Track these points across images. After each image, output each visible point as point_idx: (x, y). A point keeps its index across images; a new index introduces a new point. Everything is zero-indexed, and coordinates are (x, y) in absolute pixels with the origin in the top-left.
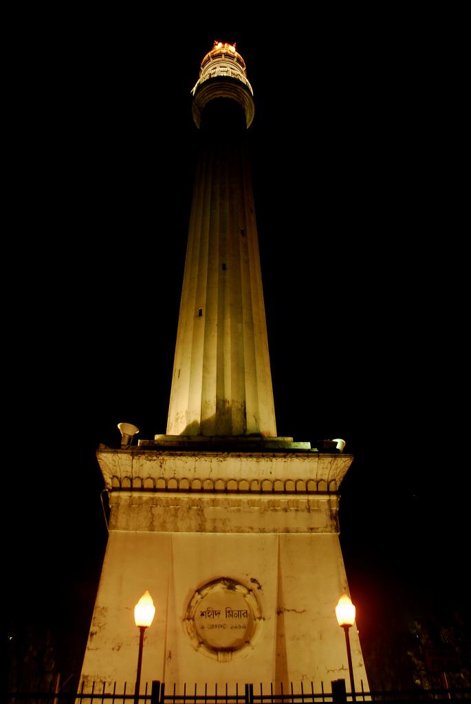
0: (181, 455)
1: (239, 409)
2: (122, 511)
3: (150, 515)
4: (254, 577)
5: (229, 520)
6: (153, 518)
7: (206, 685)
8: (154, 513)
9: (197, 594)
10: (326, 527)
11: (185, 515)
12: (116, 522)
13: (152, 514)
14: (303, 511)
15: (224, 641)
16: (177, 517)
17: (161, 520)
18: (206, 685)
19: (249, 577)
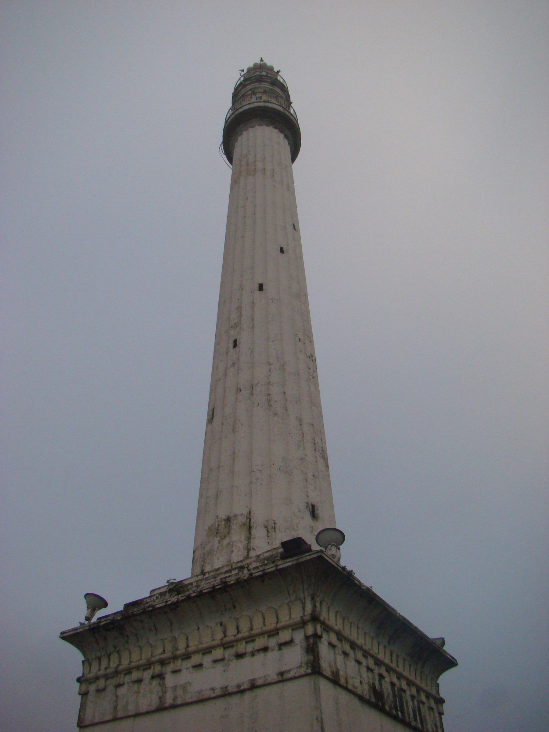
1: (244, 524)
6: (116, 701)
16: (140, 692)
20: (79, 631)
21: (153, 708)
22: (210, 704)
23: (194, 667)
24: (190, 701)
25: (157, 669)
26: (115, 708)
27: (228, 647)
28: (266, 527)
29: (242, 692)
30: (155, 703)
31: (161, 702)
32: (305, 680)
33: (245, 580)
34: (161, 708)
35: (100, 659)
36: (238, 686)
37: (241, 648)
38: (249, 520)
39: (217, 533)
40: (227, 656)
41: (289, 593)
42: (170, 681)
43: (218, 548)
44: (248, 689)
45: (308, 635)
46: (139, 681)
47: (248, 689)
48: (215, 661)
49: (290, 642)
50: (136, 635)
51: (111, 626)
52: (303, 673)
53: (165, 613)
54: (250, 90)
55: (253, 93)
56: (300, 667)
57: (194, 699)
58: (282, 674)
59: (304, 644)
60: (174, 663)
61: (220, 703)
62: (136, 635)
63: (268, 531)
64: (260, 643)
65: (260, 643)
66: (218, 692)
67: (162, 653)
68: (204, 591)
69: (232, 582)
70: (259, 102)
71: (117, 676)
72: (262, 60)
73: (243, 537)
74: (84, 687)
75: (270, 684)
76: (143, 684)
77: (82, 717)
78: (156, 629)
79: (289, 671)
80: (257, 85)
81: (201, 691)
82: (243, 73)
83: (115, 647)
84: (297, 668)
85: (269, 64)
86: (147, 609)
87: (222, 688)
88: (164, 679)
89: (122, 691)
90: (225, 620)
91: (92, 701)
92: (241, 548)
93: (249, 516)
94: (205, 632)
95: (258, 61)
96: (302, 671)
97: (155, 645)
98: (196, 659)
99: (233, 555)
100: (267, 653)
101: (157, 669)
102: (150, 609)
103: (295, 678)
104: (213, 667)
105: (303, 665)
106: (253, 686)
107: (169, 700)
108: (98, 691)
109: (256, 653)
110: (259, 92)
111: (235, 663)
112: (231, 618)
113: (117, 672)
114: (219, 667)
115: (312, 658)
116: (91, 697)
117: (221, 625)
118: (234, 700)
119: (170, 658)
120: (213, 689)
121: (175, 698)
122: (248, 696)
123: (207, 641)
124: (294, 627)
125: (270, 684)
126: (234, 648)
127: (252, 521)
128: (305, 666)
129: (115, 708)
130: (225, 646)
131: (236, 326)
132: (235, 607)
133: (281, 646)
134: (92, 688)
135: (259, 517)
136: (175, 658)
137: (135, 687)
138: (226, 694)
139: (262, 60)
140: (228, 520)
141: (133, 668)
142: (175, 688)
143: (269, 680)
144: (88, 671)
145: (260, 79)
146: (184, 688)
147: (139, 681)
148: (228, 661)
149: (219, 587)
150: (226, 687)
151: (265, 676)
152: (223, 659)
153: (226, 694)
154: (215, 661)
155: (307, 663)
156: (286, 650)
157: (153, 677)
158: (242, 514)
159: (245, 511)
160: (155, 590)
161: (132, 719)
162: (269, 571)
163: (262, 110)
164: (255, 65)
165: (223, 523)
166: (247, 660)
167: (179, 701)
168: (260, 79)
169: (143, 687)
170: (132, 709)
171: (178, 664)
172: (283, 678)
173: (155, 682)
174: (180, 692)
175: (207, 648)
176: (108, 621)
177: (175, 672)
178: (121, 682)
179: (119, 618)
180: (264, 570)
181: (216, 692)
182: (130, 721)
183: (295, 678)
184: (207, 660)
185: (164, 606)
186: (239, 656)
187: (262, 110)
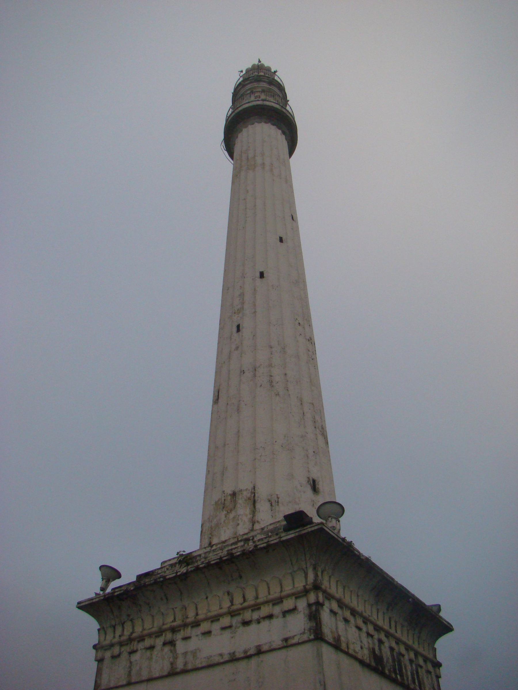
5: (200, 651)
6: (130, 667)
10: (304, 633)
13: (131, 662)
15: (328, 506)
20: (94, 601)
21: (165, 673)
24: (200, 666)
25: (169, 636)
28: (269, 501)
29: (249, 657)
30: (167, 668)
34: (173, 673)
35: (114, 627)
37: (247, 615)
38: (253, 495)
39: (223, 508)
42: (181, 647)
43: (224, 521)
49: (294, 610)
52: (307, 639)
53: (176, 583)
54: (249, 89)
56: (304, 633)
57: (204, 664)
58: (286, 640)
59: (307, 612)
61: (229, 668)
63: (271, 505)
64: (265, 610)
65: (265, 610)
66: (226, 658)
69: (239, 553)
72: (260, 61)
76: (155, 650)
78: (167, 599)
79: (293, 637)
80: (255, 85)
81: (211, 656)
83: (129, 616)
84: (301, 634)
87: (230, 654)
88: (174, 645)
89: (135, 657)
93: (253, 491)
94: (214, 601)
95: (256, 63)
96: (305, 637)
97: (167, 615)
101: (169, 636)
103: (298, 644)
105: (306, 631)
106: (259, 652)
107: (180, 665)
113: (130, 640)
114: (227, 634)
116: (107, 662)
118: (243, 664)
119: (180, 626)
120: (221, 655)
121: (185, 664)
122: (254, 661)
123: (215, 610)
124: (297, 596)
126: (241, 616)
128: (308, 633)
130: (232, 614)
132: (241, 577)
133: (285, 613)
135: (263, 492)
136: (185, 625)
137: (148, 653)
138: (233, 659)
139: (260, 61)
140: (234, 494)
141: (146, 636)
142: (185, 654)
143: (274, 646)
146: (194, 653)
150: (234, 653)
151: (270, 642)
152: (230, 627)
153: (233, 659)
155: (310, 630)
156: (289, 618)
157: (165, 644)
159: (250, 486)
162: (272, 542)
164: (254, 66)
165: (229, 497)
166: (253, 627)
167: (190, 667)
169: (156, 653)
170: (145, 675)
171: (188, 631)
172: (287, 644)
173: (167, 649)
177: (186, 639)
178: (135, 649)
179: (132, 588)
180: (268, 541)
181: (224, 657)
183: (298, 644)
184: (216, 627)
186: (246, 623)
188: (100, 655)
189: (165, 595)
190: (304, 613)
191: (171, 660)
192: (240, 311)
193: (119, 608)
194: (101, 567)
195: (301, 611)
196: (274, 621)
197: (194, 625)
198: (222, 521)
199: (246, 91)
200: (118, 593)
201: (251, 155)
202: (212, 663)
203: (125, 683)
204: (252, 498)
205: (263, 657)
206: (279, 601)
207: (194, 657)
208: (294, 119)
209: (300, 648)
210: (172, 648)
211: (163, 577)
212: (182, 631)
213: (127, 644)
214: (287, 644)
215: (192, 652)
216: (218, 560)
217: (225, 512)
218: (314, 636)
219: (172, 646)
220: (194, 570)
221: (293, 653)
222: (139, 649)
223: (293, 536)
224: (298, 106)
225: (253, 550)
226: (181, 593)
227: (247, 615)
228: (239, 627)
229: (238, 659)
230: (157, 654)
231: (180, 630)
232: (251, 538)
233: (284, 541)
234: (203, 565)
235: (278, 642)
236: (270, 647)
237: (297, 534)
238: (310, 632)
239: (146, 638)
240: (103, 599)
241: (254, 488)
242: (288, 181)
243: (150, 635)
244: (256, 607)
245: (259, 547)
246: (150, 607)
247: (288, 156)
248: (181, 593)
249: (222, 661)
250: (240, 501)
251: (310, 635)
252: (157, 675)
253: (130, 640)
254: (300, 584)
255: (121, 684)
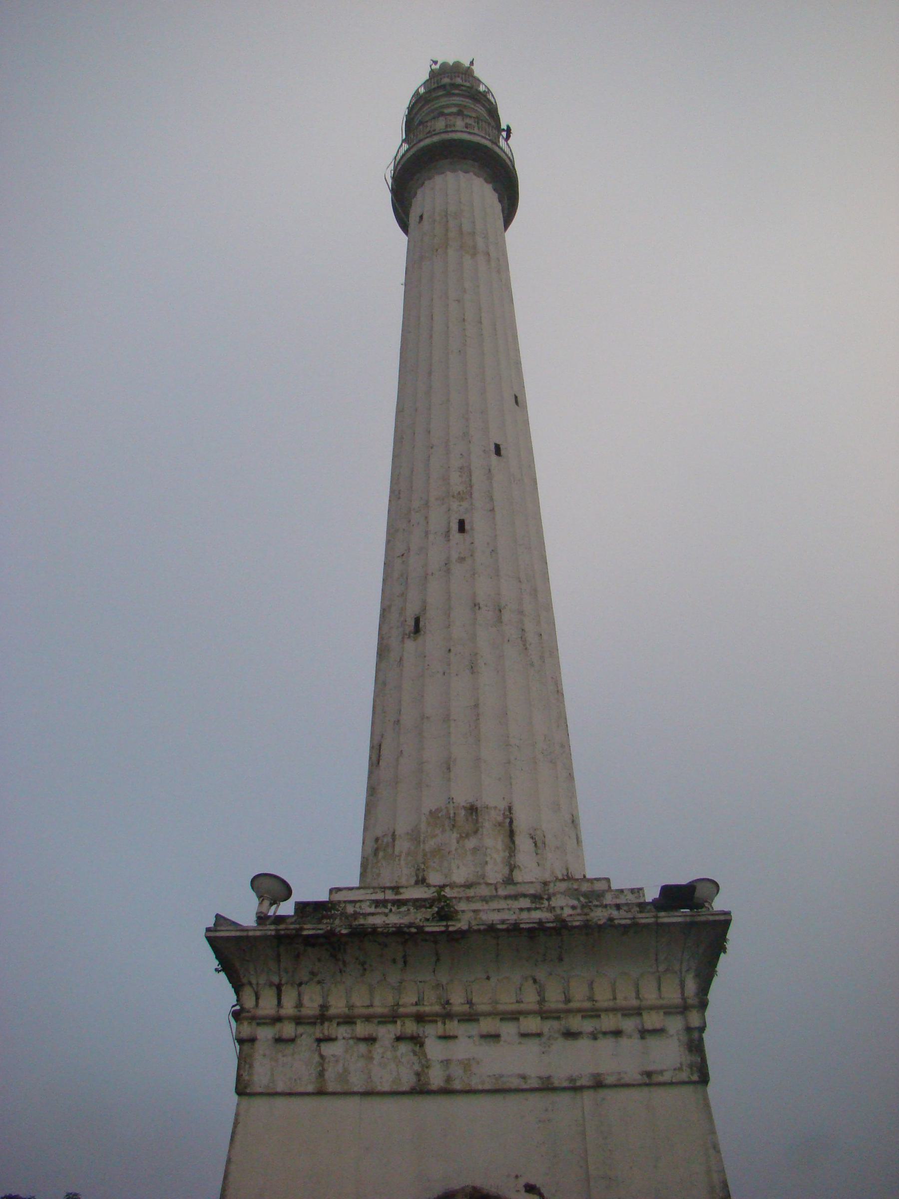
0: (370, 758)
1: (500, 824)
2: (261, 1052)
3: (317, 1058)
4: (532, 1182)
5: (478, 1063)
6: (322, 1065)
7: (516, 397)
8: (324, 1053)
9: (368, 903)
10: (680, 1069)
11: (389, 1054)
12: (250, 1074)
13: (322, 1057)
14: (630, 1037)
15: (709, 885)
16: (372, 1058)
17: (340, 1068)
18: (516, 397)
19: (522, 1182)
20: (251, 934)
21: (405, 1088)
22: (512, 1099)
23: (483, 1036)
24: (480, 1087)
25: (411, 1027)
26: (321, 1074)
27: (547, 1018)
28: (532, 838)
29: (575, 1089)
30: (407, 1080)
31: (419, 1080)
32: (691, 1088)
33: (600, 926)
34: (420, 1090)
35: (279, 988)
36: (572, 1079)
37: (576, 1023)
38: (508, 820)
39: (454, 826)
40: (546, 1030)
41: (656, 960)
42: (434, 1049)
43: (456, 850)
44: (589, 1087)
45: (692, 1026)
46: (371, 1040)
47: (589, 1087)
48: (524, 1035)
49: (659, 1032)
50: (363, 964)
51: (322, 940)
52: (687, 1079)
53: (436, 942)
54: (455, 105)
55: (460, 113)
56: (680, 1069)
57: (487, 1086)
58: (649, 1074)
59: (684, 1038)
60: (444, 1023)
61: (536, 1101)
62: (363, 964)
63: (536, 845)
64: (608, 1022)
65: (608, 1022)
66: (535, 1083)
67: (416, 1004)
68: (522, 926)
69: (577, 923)
70: (485, 138)
71: (322, 1023)
72: (472, 63)
73: (500, 846)
74: (247, 1030)
75: (627, 1085)
76: (377, 1045)
77: (246, 1077)
78: (405, 963)
79: (661, 1072)
80: (468, 102)
81: (501, 1076)
82: (434, 67)
83: (313, 974)
84: (675, 1069)
85: (477, 74)
86: (406, 930)
87: (540, 1078)
88: (422, 1045)
89: (328, 1049)
90: (541, 975)
91: (264, 1055)
92: (499, 860)
93: (507, 813)
94: (505, 986)
95: (467, 64)
96: (684, 1076)
97: (415, 990)
98: (487, 1025)
99: (489, 868)
100: (619, 1039)
101: (411, 1027)
102: (413, 930)
103: (671, 1084)
104: (520, 1043)
105: (684, 1068)
106: (598, 1084)
107: (436, 1078)
108: (279, 1040)
109: (600, 1036)
110: (471, 117)
111: (560, 1044)
112: (551, 974)
113: (322, 1017)
114: (533, 1046)
115: (699, 1059)
116: (262, 1048)
117: (535, 981)
118: (565, 1098)
119: (437, 1015)
120: (524, 1077)
121: (449, 1079)
122: (588, 1097)
123: (507, 1002)
124: (668, 1010)
125: (627, 1085)
126: (563, 1022)
127: (515, 823)
128: (689, 1070)
129: (321, 1074)
130: (545, 1014)
131: (460, 497)
132: (561, 959)
133: (644, 1033)
134: (265, 1034)
135: (522, 822)
136: (448, 1016)
137: (363, 1047)
138: (547, 1087)
139: (472, 63)
140: (472, 810)
141: (360, 1016)
142: (446, 1063)
143: (627, 1079)
144: (254, 1003)
145: (449, 90)
146: (466, 1065)
147: (371, 1040)
148: (549, 1039)
149: (551, 925)
150: (549, 1078)
151: (619, 1073)
152: (539, 1035)
153: (547, 1087)
154: (524, 1035)
155: (691, 1066)
156: (653, 1042)
157: (399, 1039)
158: (495, 808)
159: (502, 805)
160: (338, 890)
161: (357, 1099)
162: (643, 921)
163: (453, 145)
164: (457, 65)
165: (463, 812)
166: (583, 1044)
167: (457, 1085)
168: (449, 90)
169: (380, 1050)
170: (357, 1082)
171: (453, 1027)
172: (649, 1080)
173: (404, 1048)
174: (457, 1071)
175: (512, 1013)
176: (320, 932)
177: (445, 1037)
178: (334, 1036)
179: (344, 931)
180: (634, 918)
181: (529, 1081)
182: (352, 1103)
183: (671, 1084)
184: (508, 1030)
185: (442, 932)
186: (570, 1035)
187: (453, 145)
188: (247, 1030)
189: (404, 957)
190: (679, 1040)
191: (417, 1067)
192: (466, 495)
193: (298, 956)
194: (253, 881)
195: (672, 1036)
196: (624, 1042)
197: (341, 1020)
198: (453, 849)
199: (448, 106)
200: (311, 932)
201: (466, 227)
202: (505, 1086)
203: (310, 1088)
204: (507, 824)
205: (603, 1093)
206: (638, 1012)
207: (465, 1071)
208: (514, 166)
209: (674, 1091)
210: (417, 1048)
211: (416, 927)
212: (439, 1024)
213: (314, 1024)
214: (649, 1080)
215: (460, 1062)
216: (535, 925)
217: (455, 835)
218: (699, 1077)
219: (416, 1044)
220: (485, 930)
221: (659, 1096)
222: (340, 1037)
223: (680, 920)
224: (524, 152)
225: (605, 923)
226: (438, 960)
227: (576, 1023)
228: (557, 1038)
229: (554, 1089)
230: (383, 1053)
231: (436, 1021)
232: (546, 897)
233: (663, 924)
234: (504, 926)
235: (632, 1073)
236: (619, 1080)
237: (688, 919)
238: (691, 1068)
239: (358, 1021)
240: (274, 937)
241: (510, 809)
242: (501, 267)
243: (368, 1018)
244: (594, 1013)
245: (616, 922)
246: (365, 969)
247: (501, 222)
248: (438, 960)
249: (525, 1086)
250: (487, 826)
251: (692, 1074)
252: (386, 1088)
253: (322, 1017)
254: (672, 995)
255: (301, 1089)
